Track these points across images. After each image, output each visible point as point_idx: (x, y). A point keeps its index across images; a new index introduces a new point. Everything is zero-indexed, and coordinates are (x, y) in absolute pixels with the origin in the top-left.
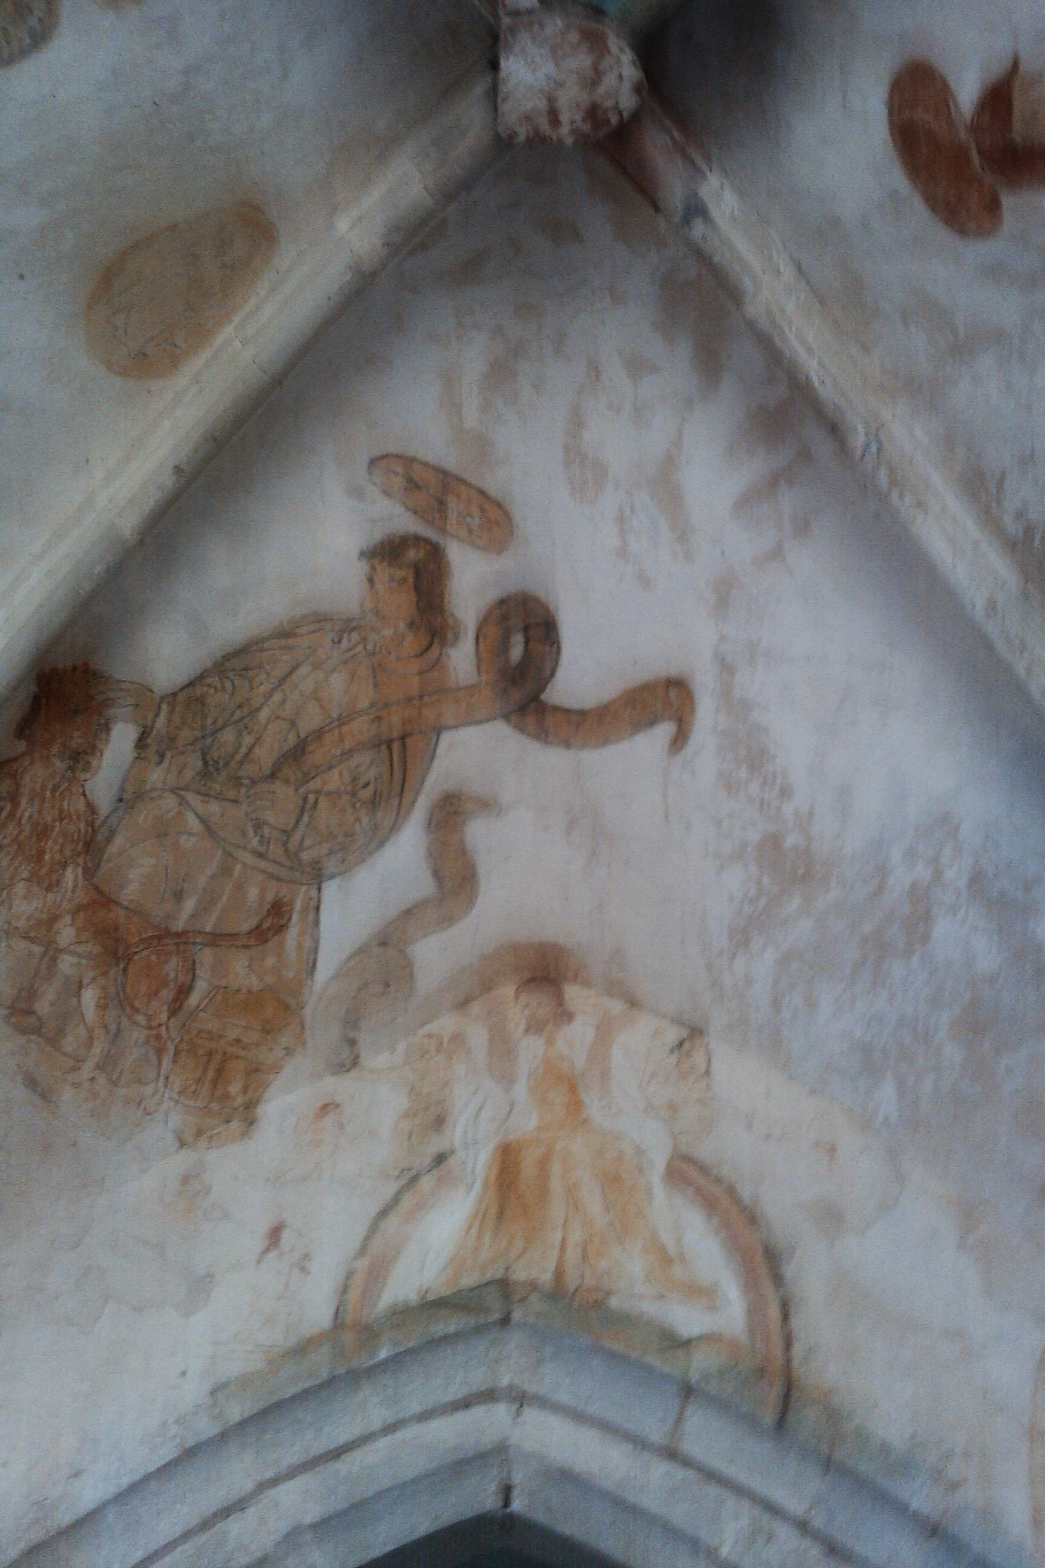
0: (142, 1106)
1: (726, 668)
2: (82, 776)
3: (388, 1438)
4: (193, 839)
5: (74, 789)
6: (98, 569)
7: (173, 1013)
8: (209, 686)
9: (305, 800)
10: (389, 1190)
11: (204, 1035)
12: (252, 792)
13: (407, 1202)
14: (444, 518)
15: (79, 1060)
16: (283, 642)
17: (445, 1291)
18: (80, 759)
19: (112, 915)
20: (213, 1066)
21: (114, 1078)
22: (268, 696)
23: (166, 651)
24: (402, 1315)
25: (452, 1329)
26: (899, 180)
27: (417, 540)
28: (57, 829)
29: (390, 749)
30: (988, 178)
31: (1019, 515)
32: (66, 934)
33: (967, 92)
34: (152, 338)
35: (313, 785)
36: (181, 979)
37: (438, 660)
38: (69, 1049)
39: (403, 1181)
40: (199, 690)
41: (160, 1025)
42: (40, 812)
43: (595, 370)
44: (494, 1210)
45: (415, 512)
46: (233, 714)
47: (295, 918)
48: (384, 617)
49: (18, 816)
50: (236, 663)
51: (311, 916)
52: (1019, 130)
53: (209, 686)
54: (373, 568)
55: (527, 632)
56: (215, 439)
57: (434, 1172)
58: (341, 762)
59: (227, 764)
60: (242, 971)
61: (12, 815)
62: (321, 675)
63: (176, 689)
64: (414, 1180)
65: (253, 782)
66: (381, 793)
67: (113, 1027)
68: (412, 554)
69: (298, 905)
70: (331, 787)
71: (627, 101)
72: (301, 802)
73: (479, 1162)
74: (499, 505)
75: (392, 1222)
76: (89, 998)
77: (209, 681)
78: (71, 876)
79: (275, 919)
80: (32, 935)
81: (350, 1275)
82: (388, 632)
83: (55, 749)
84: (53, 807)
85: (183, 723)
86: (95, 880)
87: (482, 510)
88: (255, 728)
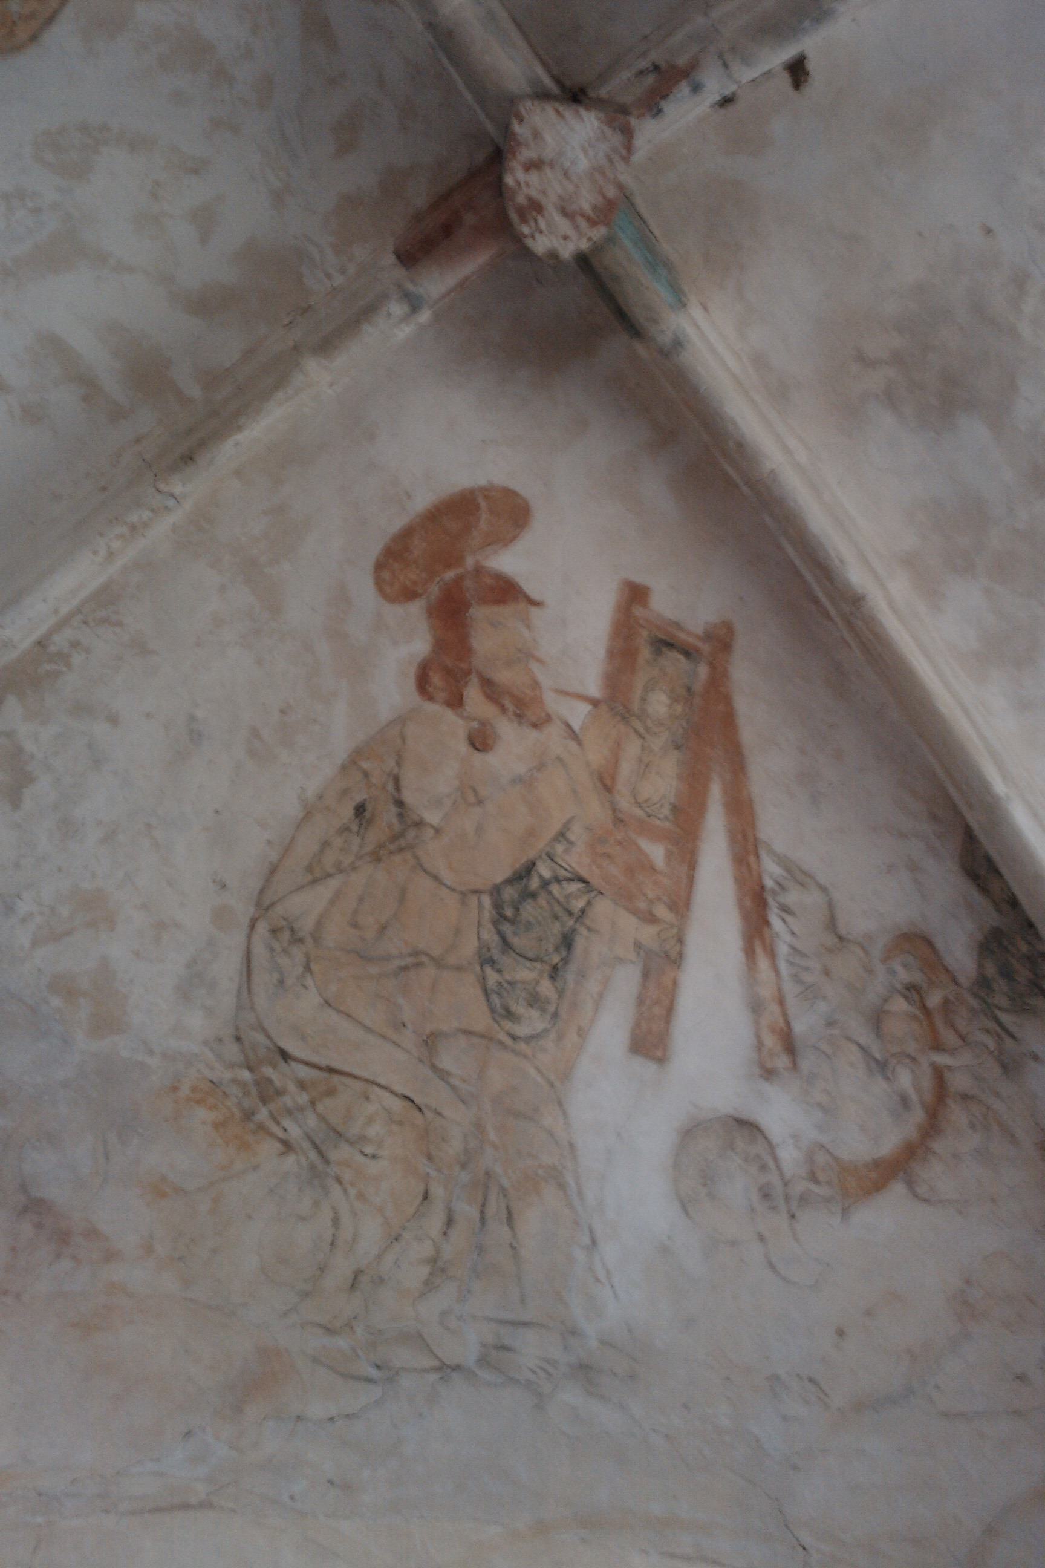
26: (422, 501)
30: (435, 590)
31: (75, 644)
33: (507, 562)
43: (197, 168)
52: (479, 613)
71: (540, 245)
74: (34, 38)
87: (32, 16)
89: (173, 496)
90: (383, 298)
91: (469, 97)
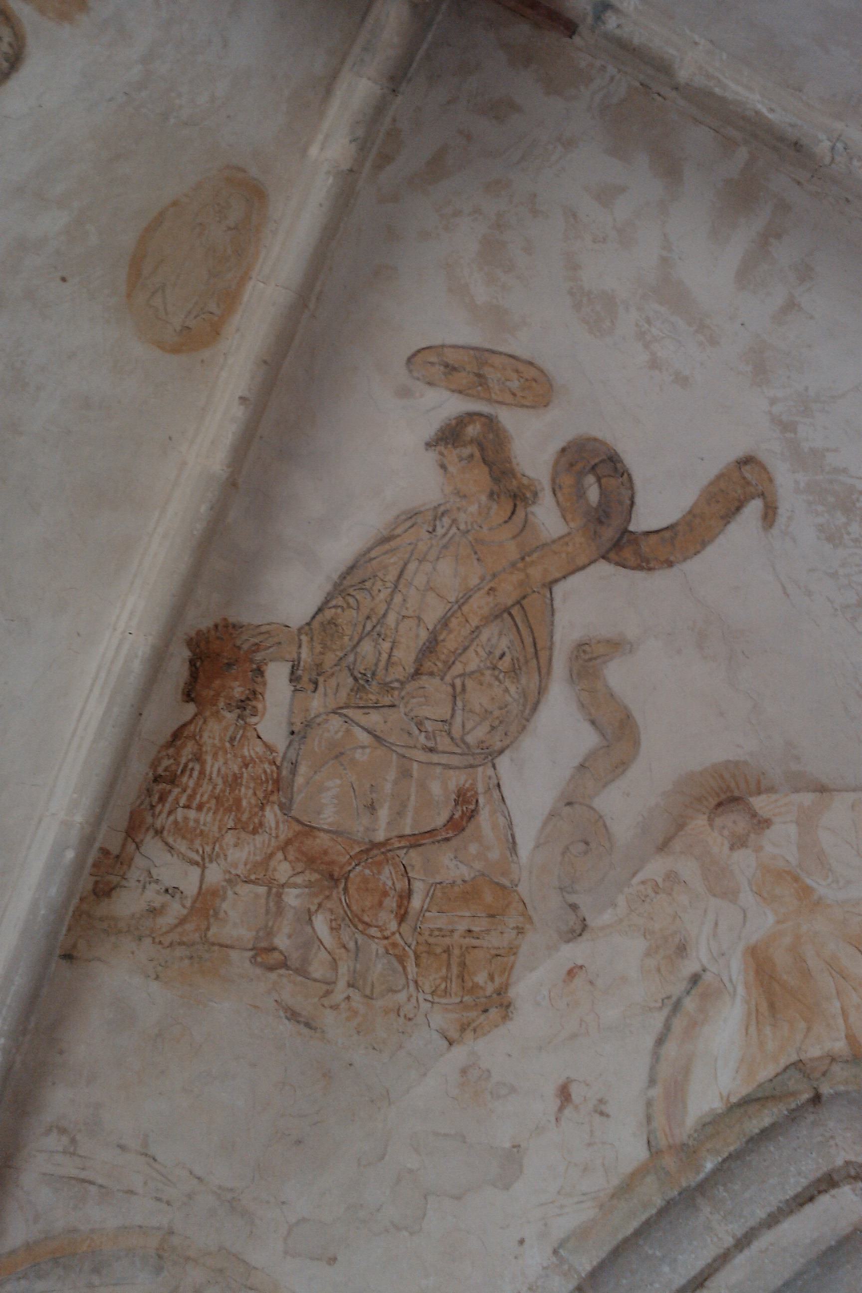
0: (402, 1014)
1: (787, 427)
2: (253, 720)
3: (747, 1253)
4: (368, 751)
5: (249, 734)
6: (203, 509)
7: (402, 918)
8: (335, 607)
9: (453, 686)
10: (657, 1021)
11: (437, 933)
12: (403, 693)
13: (678, 1024)
14: (488, 389)
15: (330, 984)
16: (387, 547)
17: (744, 1091)
18: (246, 706)
19: (318, 841)
20: (455, 961)
21: (368, 992)
22: (389, 603)
23: (290, 595)
24: (713, 1125)
25: (767, 1121)
27: (472, 416)
28: (245, 775)
29: (510, 614)
32: (283, 870)
34: (190, 312)
35: (458, 668)
36: (398, 886)
37: (526, 521)
38: (317, 975)
39: (666, 1012)
40: (328, 614)
41: (393, 934)
42: (226, 763)
43: (572, 215)
44: (764, 1007)
45: (460, 392)
46: (364, 627)
47: (481, 801)
48: (465, 496)
49: (208, 772)
50: (351, 582)
51: (496, 794)
53: (335, 607)
54: (441, 454)
55: (596, 466)
56: (265, 362)
57: (693, 992)
58: (472, 640)
59: (374, 674)
60: (451, 865)
61: (202, 773)
62: (427, 567)
63: (308, 619)
64: (677, 1006)
65: (402, 683)
66: (518, 659)
67: (351, 945)
68: (472, 430)
69: (480, 788)
70: (472, 667)
72: (450, 689)
73: (736, 969)
75: (671, 1048)
76: (321, 923)
77: (334, 603)
78: (271, 815)
79: (464, 812)
80: (253, 877)
81: (649, 1104)
82: (473, 509)
83: (221, 704)
84: (235, 756)
85: (325, 646)
86: (293, 813)
88: (388, 632)
89: (833, 148)
90: (608, 37)
91: (430, 37)
